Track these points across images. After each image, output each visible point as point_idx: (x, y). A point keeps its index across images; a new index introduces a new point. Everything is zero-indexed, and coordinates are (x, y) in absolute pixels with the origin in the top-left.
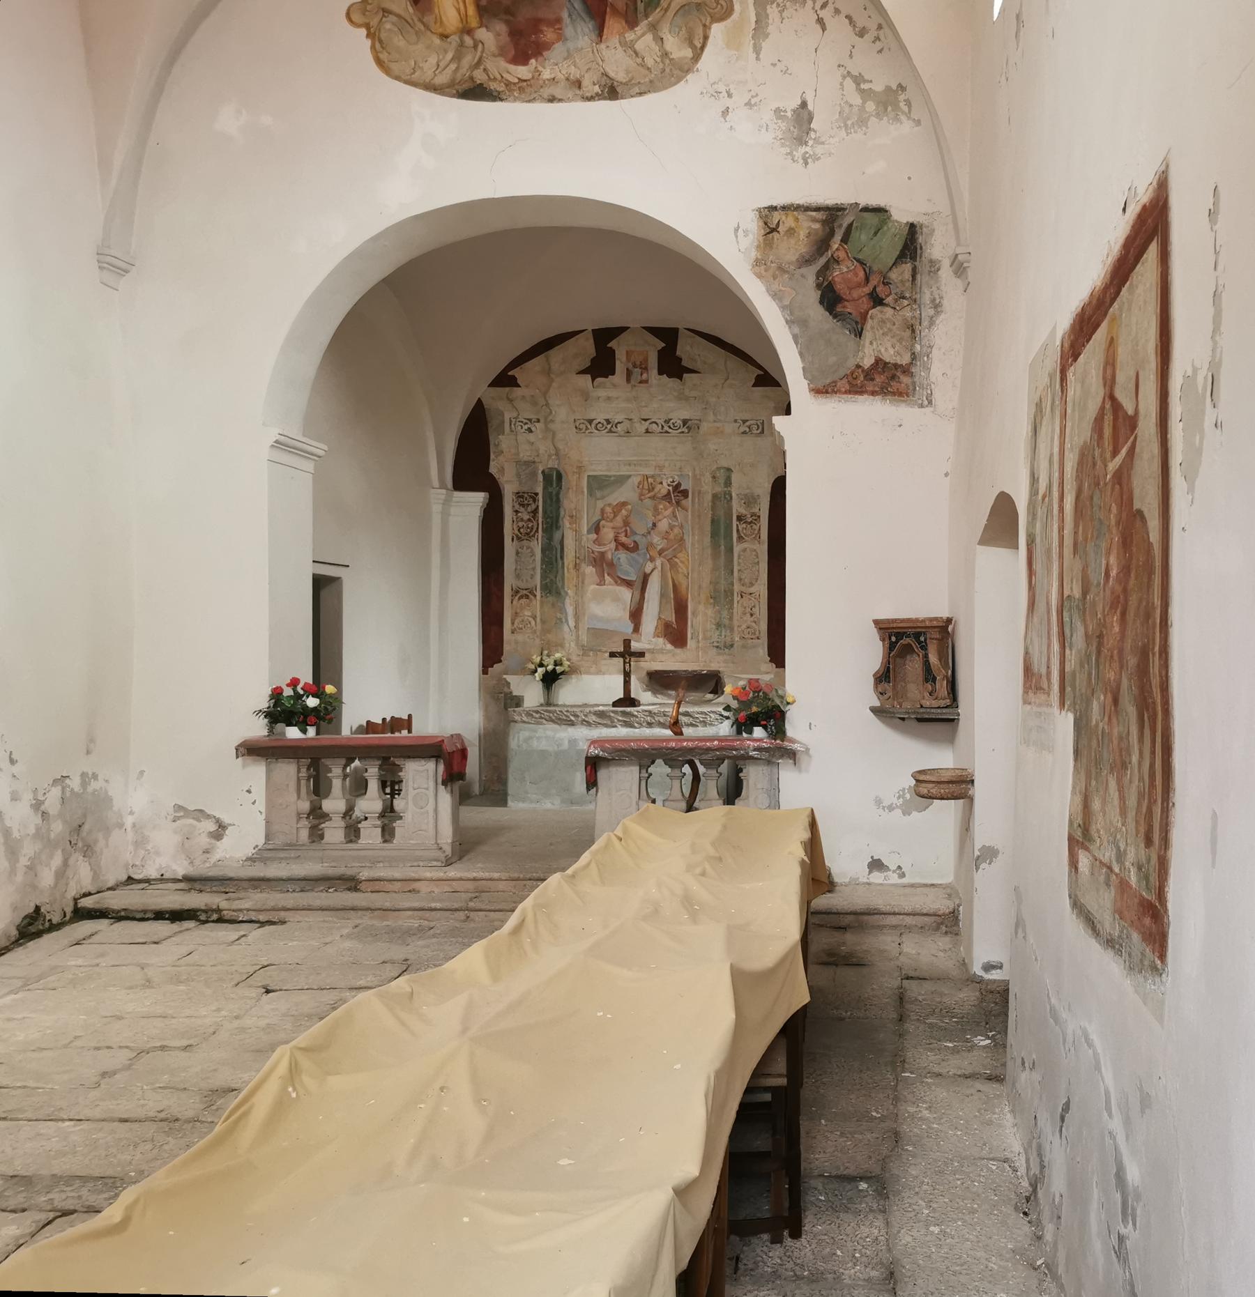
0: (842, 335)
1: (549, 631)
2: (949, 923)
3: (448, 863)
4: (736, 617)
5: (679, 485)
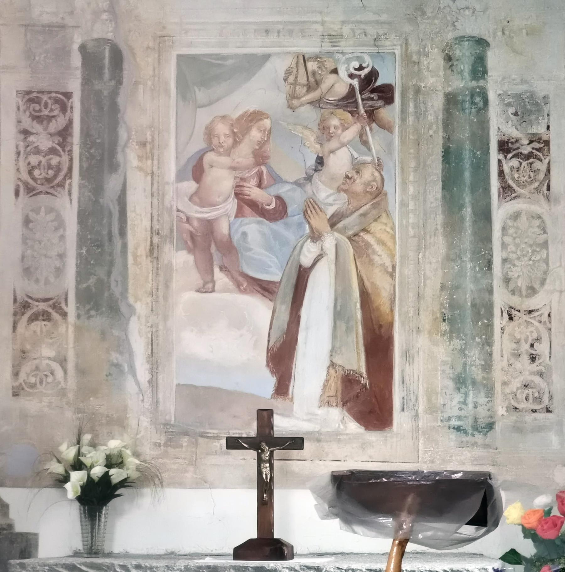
1: (94, 392)
4: (499, 363)
5: (373, 74)
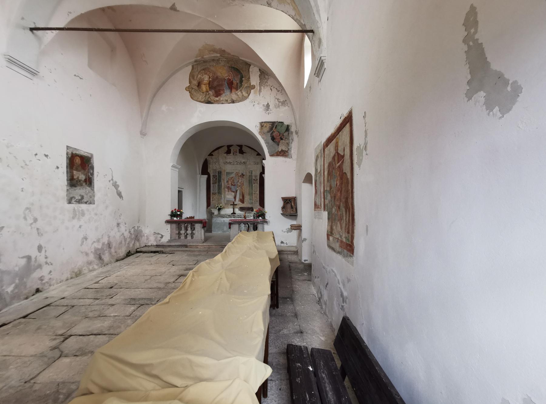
0: (276, 145)
2: (296, 253)
3: (203, 243)
